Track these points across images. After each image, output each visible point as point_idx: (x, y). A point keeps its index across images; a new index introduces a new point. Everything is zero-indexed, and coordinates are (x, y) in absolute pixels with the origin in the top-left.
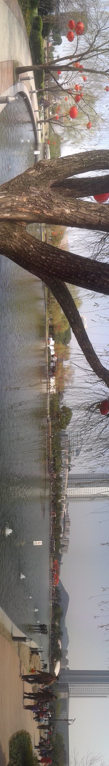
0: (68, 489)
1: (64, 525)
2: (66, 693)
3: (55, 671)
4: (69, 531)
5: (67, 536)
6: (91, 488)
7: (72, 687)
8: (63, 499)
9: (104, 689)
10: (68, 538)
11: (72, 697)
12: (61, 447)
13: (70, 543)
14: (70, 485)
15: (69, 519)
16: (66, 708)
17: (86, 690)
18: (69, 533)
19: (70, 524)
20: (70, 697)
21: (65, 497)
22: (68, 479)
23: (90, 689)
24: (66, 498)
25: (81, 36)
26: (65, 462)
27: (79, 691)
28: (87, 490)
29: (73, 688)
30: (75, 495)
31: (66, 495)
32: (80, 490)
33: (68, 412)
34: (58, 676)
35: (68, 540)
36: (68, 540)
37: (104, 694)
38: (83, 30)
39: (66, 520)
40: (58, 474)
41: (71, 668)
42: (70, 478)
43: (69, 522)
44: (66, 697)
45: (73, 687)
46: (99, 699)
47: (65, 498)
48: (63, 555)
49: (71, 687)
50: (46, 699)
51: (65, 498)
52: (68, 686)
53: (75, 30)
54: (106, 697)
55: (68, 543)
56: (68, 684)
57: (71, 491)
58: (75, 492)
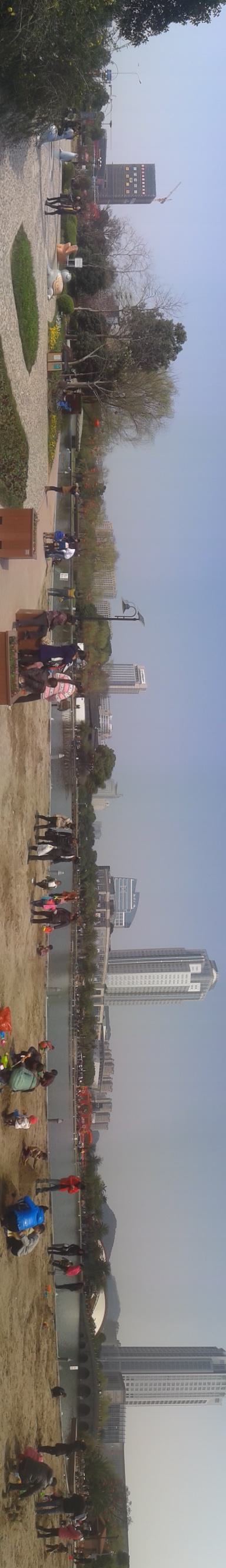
0: (110, 976)
1: (101, 1060)
2: (119, 1392)
3: (93, 1316)
4: (112, 1083)
5: (109, 1095)
6: (155, 974)
7: (130, 1382)
8: (97, 994)
9: (196, 1384)
10: (108, 1099)
11: (131, 1403)
12: (123, 34)
13: (113, 1107)
14: (112, 969)
15: (112, 1059)
16: (118, 1425)
17: (162, 1386)
18: (111, 1087)
19: (113, 1069)
20: (127, 1403)
21: (102, 990)
22: (109, 958)
23: (169, 1384)
24: (105, 992)
25: (117, 270)
26: (103, 915)
27: (146, 1390)
28: (152, 978)
29: (133, 1382)
30: (124, 988)
31: (105, 987)
32: (133, 979)
33: (88, 1225)
34: (102, 1332)
35: (110, 1103)
36: (110, 1103)
37: (199, 1395)
38: (115, 374)
39: (103, 1080)
40: (104, 347)
41: (124, 1344)
42: (114, 956)
43: (111, 1064)
44: (119, 1400)
45: (132, 1382)
46: (190, 1406)
47: (102, 994)
48: (101, 1137)
49: (128, 1382)
50: (64, 23)
51: (102, 994)
52: (122, 1379)
53: (83, 1170)
54: (205, 1402)
55: (111, 1107)
56: (123, 1375)
57: (116, 981)
58: (122, 981)
